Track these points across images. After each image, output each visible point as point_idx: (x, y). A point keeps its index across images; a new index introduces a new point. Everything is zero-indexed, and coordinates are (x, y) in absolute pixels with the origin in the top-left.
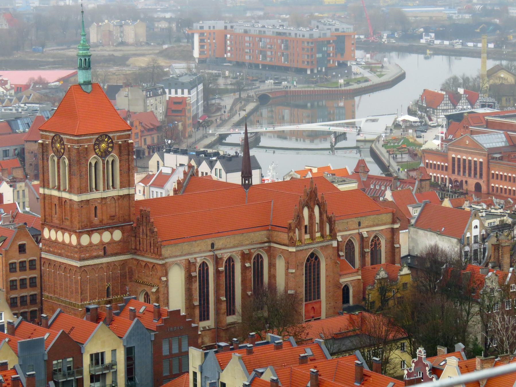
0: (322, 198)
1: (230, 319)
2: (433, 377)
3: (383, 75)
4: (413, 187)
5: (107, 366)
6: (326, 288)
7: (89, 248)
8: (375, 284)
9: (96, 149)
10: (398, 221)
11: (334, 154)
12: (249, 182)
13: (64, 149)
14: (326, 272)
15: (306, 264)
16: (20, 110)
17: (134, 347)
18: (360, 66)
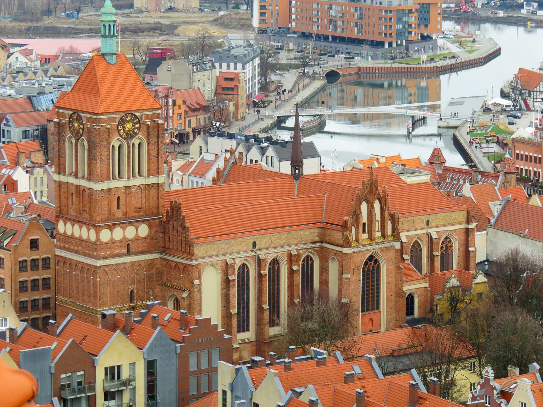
0: (384, 192)
1: (273, 331)
2: (501, 402)
3: (474, 51)
4: (497, 182)
5: (123, 382)
6: (387, 296)
7: (110, 244)
8: (444, 293)
9: (120, 130)
10: (473, 220)
11: (411, 142)
12: (299, 171)
13: (83, 129)
14: (387, 278)
15: (364, 268)
16: (44, 85)
17: (156, 360)
18: (448, 39)
